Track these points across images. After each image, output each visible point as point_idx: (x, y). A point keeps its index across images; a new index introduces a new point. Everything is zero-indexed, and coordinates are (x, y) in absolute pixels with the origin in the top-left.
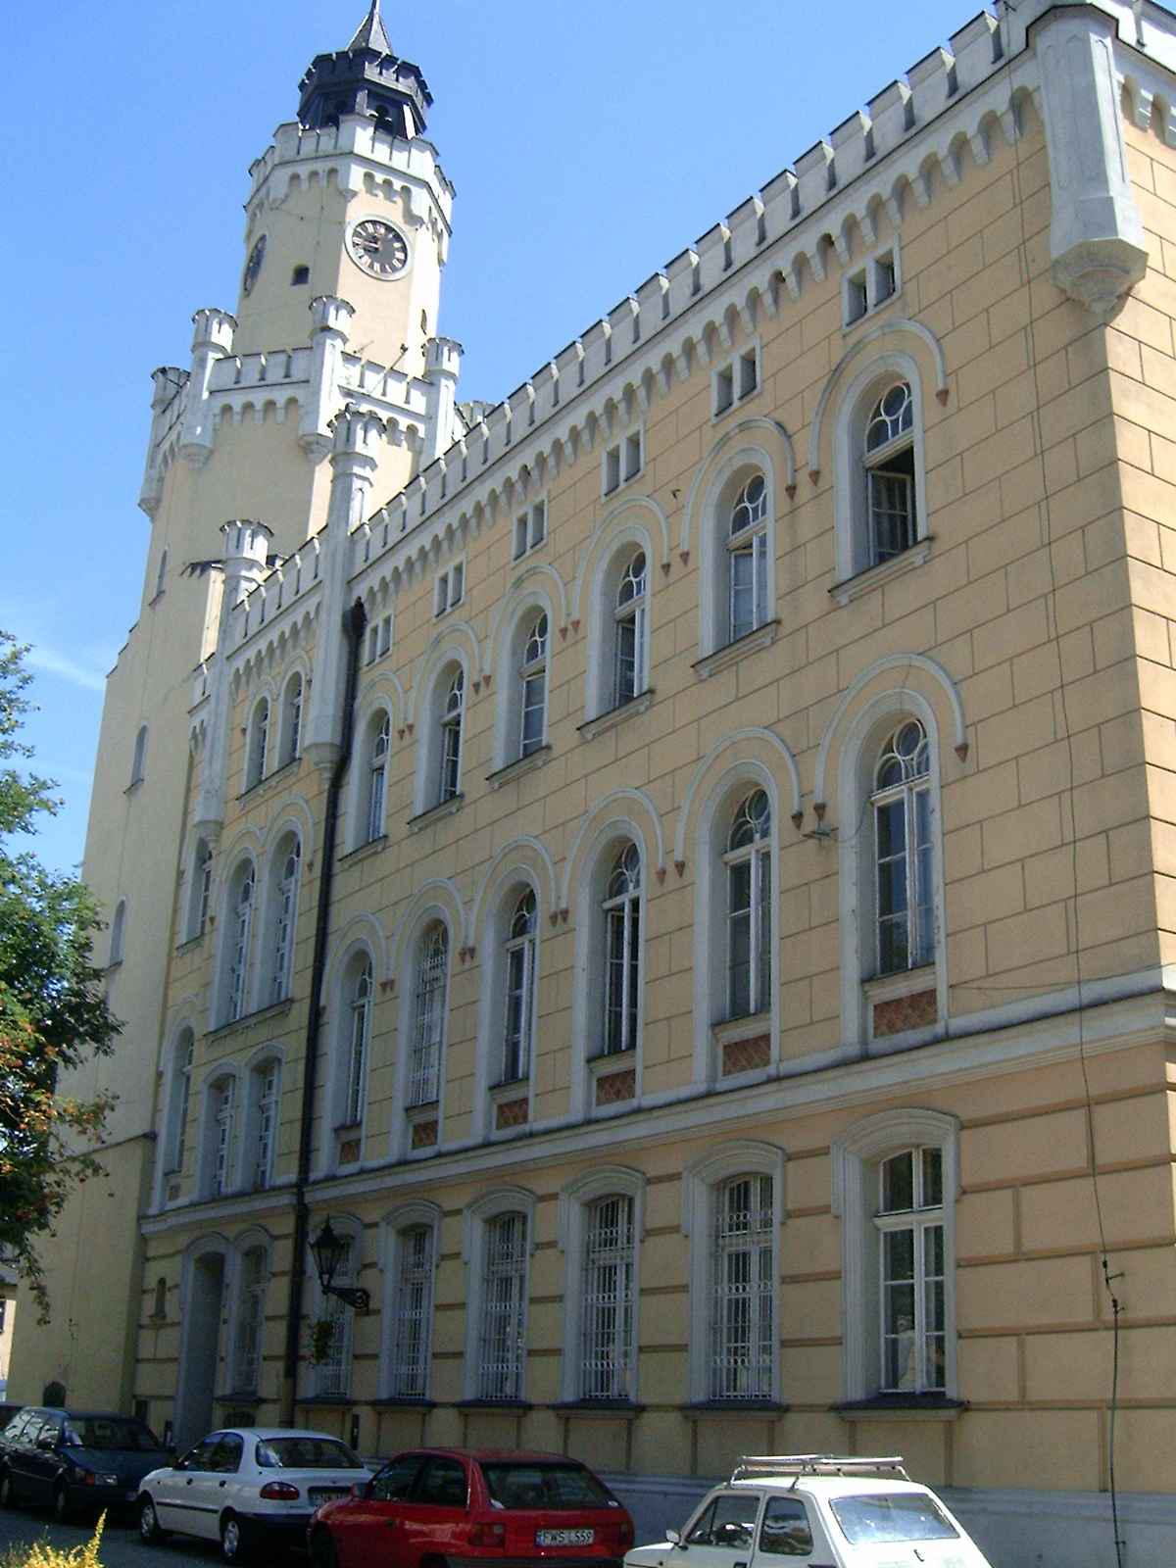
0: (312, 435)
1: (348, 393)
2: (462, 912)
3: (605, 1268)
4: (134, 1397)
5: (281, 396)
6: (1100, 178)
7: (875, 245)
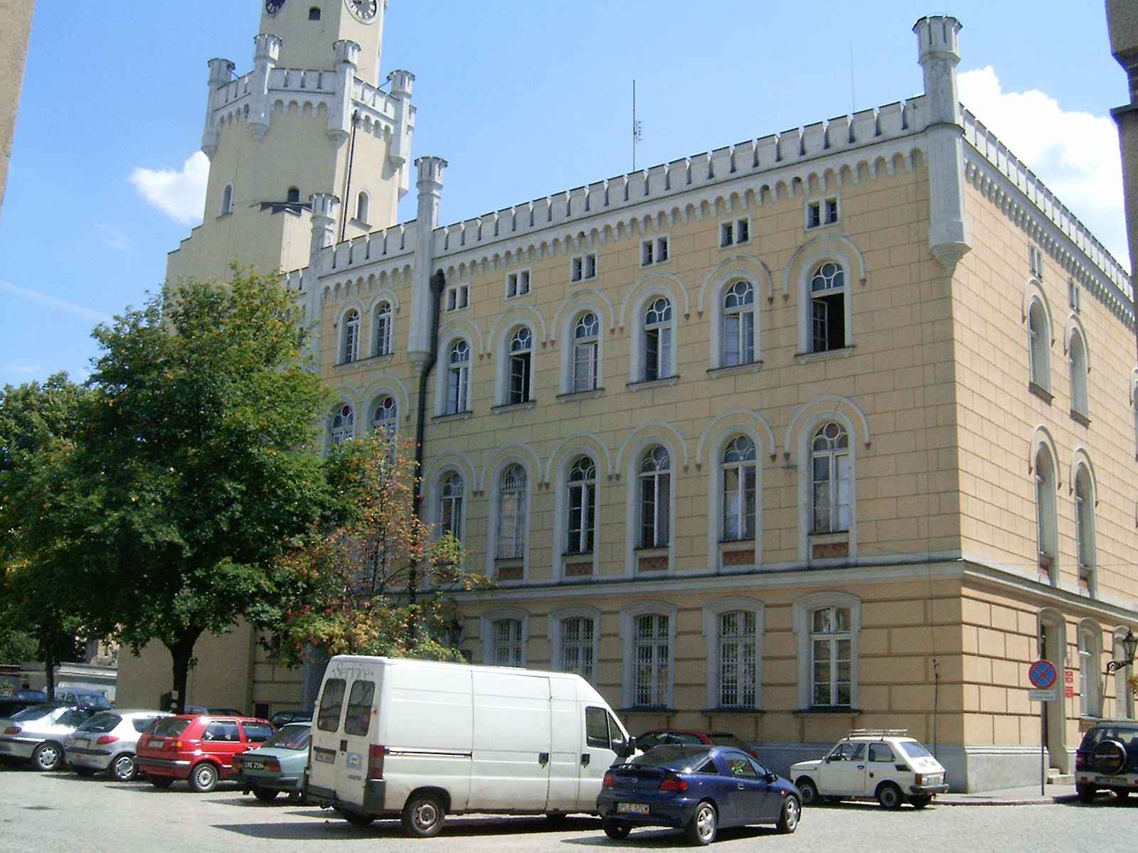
0: (339, 130)
1: (356, 104)
2: (539, 465)
3: (750, 632)
4: (254, 702)
5: (315, 101)
6: (956, 212)
7: (825, 193)
